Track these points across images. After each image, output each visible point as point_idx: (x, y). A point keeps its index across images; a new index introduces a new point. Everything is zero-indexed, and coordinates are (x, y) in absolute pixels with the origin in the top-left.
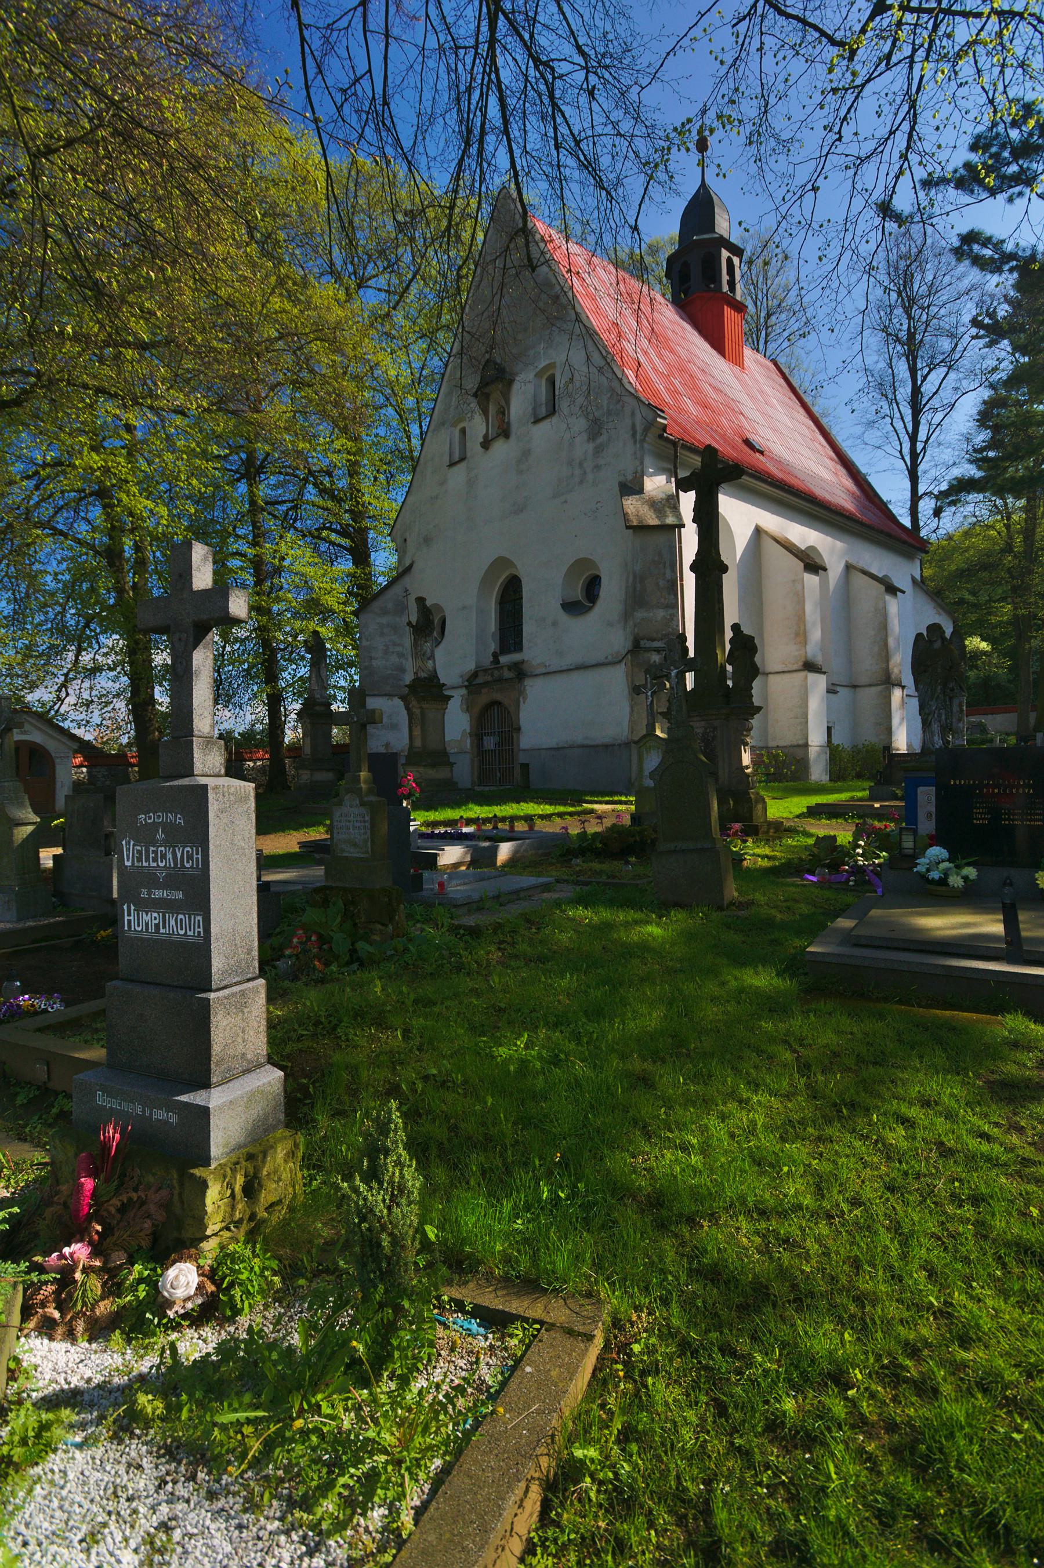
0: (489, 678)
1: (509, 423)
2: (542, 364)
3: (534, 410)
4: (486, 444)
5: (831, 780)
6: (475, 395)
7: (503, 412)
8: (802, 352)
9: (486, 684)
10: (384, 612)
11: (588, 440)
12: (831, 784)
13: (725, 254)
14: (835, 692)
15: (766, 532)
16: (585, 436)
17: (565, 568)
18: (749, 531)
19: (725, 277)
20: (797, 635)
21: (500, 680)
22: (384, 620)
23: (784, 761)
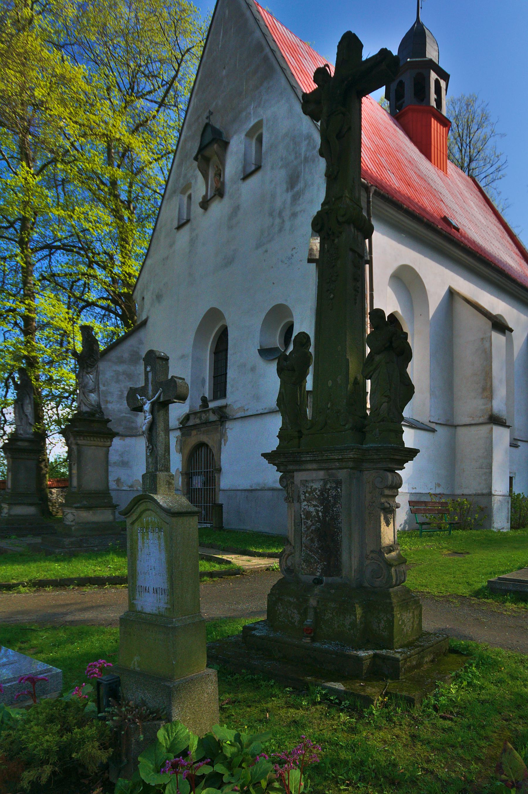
0: (198, 421)
1: (223, 184)
2: (253, 122)
3: (244, 168)
4: (205, 204)
5: (512, 528)
6: (196, 159)
7: (219, 174)
8: (495, 192)
9: (195, 426)
10: (121, 361)
11: (287, 191)
12: (512, 533)
13: (433, 76)
14: (516, 446)
15: (458, 294)
16: (285, 186)
17: (263, 315)
18: (443, 292)
19: (433, 96)
20: (484, 389)
21: (207, 423)
22: (121, 368)
23: (469, 510)
